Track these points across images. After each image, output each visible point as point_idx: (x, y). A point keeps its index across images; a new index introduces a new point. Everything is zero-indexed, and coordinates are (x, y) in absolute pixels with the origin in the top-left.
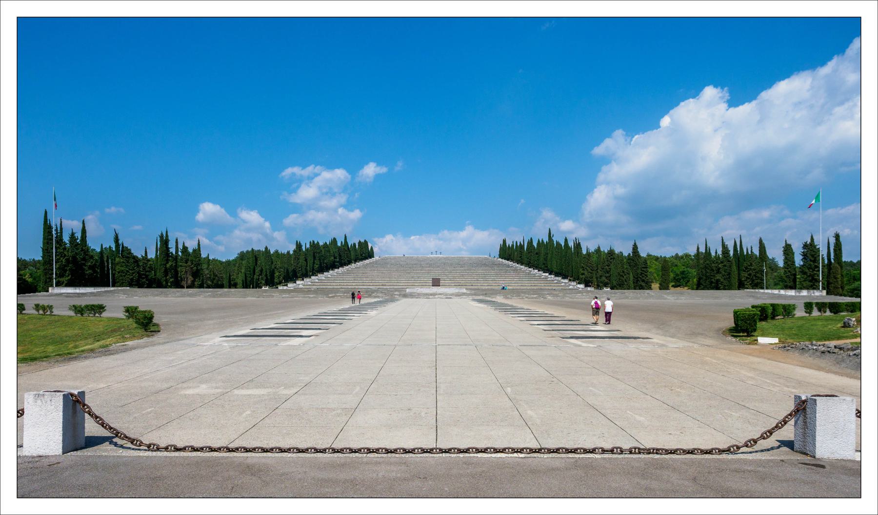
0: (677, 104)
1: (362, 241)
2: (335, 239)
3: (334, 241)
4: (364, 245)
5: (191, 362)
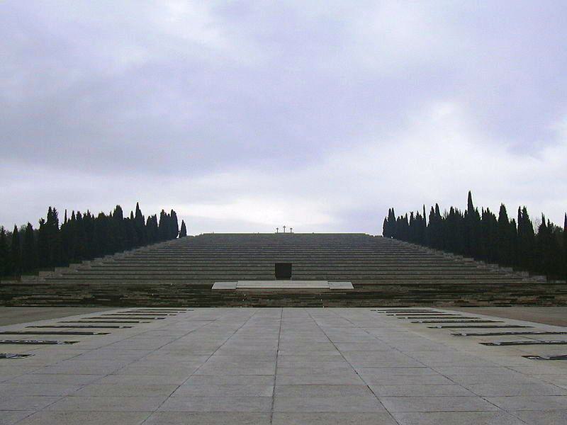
1: (168, 212)
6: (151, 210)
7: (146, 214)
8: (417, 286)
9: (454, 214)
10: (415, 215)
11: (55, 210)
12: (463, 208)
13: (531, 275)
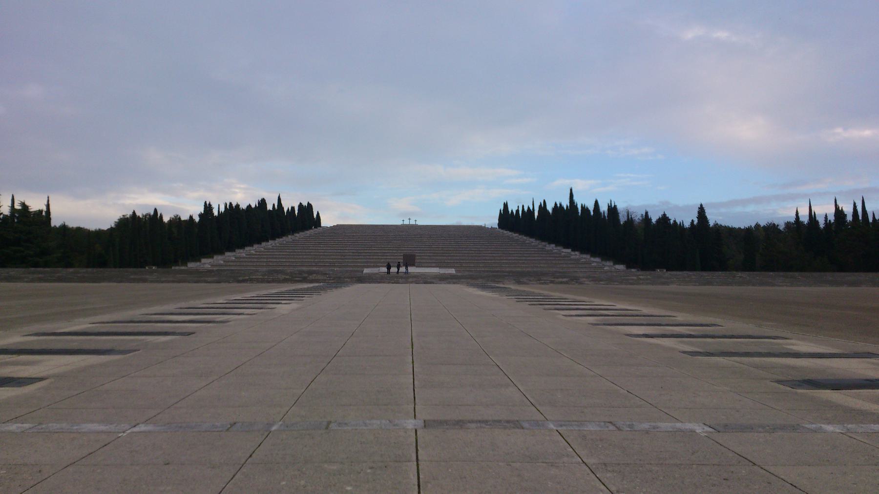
0: (79, 229)
1: (305, 204)
2: (263, 201)
3: (263, 203)
4: (306, 210)
5: (76, 393)
6: (290, 203)
7: (286, 206)
9: (557, 209)
10: (526, 209)
11: (210, 204)
12: (566, 203)
13: (615, 264)
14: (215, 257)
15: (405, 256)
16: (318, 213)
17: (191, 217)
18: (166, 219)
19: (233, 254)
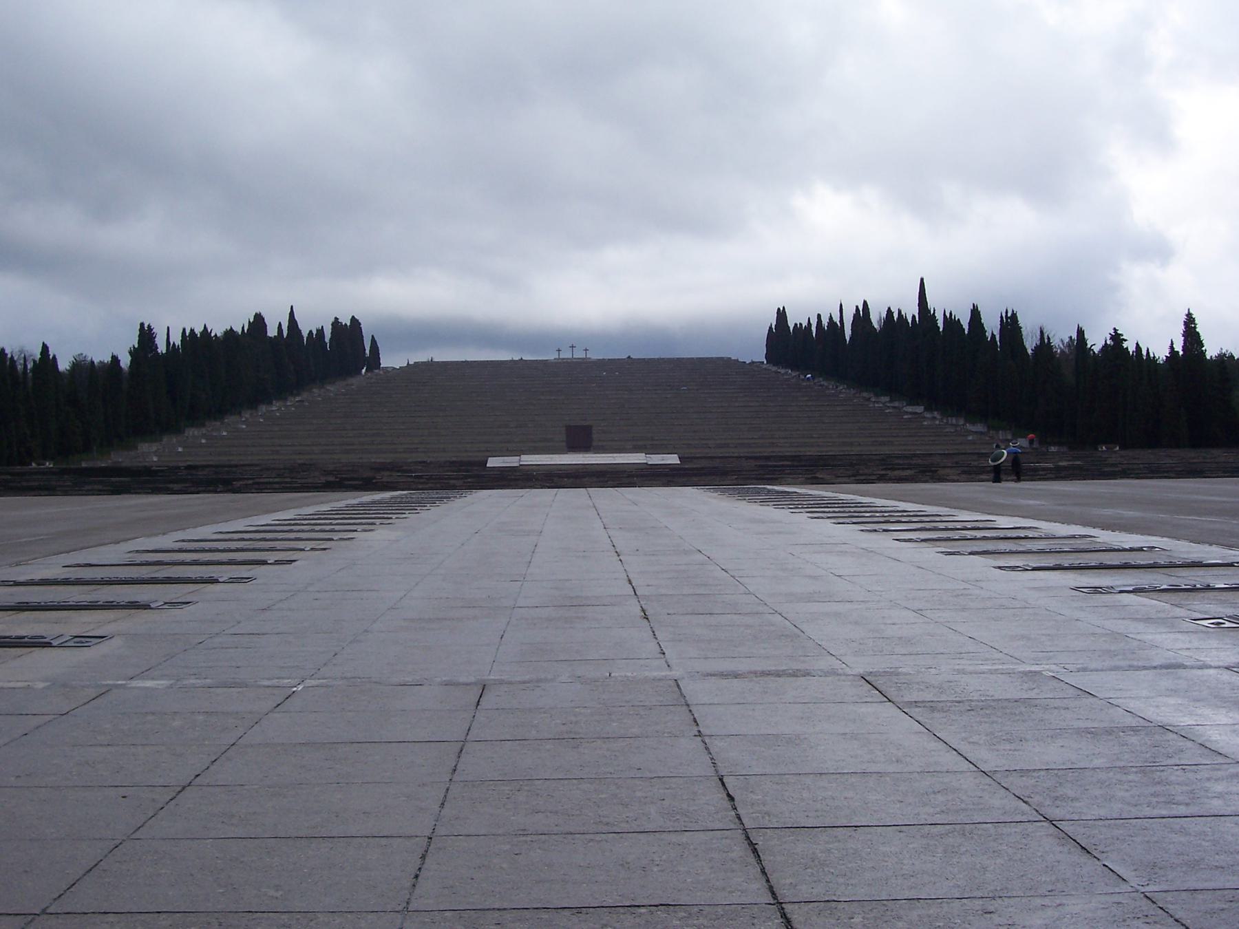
1: (346, 321)
8: (767, 458)
9: (893, 322)
10: (825, 322)
12: (911, 310)
14: (165, 439)
15: (569, 429)
16: (373, 341)
17: (115, 359)
18: (64, 365)
19: (204, 431)
